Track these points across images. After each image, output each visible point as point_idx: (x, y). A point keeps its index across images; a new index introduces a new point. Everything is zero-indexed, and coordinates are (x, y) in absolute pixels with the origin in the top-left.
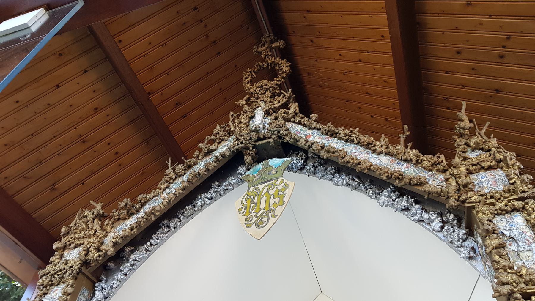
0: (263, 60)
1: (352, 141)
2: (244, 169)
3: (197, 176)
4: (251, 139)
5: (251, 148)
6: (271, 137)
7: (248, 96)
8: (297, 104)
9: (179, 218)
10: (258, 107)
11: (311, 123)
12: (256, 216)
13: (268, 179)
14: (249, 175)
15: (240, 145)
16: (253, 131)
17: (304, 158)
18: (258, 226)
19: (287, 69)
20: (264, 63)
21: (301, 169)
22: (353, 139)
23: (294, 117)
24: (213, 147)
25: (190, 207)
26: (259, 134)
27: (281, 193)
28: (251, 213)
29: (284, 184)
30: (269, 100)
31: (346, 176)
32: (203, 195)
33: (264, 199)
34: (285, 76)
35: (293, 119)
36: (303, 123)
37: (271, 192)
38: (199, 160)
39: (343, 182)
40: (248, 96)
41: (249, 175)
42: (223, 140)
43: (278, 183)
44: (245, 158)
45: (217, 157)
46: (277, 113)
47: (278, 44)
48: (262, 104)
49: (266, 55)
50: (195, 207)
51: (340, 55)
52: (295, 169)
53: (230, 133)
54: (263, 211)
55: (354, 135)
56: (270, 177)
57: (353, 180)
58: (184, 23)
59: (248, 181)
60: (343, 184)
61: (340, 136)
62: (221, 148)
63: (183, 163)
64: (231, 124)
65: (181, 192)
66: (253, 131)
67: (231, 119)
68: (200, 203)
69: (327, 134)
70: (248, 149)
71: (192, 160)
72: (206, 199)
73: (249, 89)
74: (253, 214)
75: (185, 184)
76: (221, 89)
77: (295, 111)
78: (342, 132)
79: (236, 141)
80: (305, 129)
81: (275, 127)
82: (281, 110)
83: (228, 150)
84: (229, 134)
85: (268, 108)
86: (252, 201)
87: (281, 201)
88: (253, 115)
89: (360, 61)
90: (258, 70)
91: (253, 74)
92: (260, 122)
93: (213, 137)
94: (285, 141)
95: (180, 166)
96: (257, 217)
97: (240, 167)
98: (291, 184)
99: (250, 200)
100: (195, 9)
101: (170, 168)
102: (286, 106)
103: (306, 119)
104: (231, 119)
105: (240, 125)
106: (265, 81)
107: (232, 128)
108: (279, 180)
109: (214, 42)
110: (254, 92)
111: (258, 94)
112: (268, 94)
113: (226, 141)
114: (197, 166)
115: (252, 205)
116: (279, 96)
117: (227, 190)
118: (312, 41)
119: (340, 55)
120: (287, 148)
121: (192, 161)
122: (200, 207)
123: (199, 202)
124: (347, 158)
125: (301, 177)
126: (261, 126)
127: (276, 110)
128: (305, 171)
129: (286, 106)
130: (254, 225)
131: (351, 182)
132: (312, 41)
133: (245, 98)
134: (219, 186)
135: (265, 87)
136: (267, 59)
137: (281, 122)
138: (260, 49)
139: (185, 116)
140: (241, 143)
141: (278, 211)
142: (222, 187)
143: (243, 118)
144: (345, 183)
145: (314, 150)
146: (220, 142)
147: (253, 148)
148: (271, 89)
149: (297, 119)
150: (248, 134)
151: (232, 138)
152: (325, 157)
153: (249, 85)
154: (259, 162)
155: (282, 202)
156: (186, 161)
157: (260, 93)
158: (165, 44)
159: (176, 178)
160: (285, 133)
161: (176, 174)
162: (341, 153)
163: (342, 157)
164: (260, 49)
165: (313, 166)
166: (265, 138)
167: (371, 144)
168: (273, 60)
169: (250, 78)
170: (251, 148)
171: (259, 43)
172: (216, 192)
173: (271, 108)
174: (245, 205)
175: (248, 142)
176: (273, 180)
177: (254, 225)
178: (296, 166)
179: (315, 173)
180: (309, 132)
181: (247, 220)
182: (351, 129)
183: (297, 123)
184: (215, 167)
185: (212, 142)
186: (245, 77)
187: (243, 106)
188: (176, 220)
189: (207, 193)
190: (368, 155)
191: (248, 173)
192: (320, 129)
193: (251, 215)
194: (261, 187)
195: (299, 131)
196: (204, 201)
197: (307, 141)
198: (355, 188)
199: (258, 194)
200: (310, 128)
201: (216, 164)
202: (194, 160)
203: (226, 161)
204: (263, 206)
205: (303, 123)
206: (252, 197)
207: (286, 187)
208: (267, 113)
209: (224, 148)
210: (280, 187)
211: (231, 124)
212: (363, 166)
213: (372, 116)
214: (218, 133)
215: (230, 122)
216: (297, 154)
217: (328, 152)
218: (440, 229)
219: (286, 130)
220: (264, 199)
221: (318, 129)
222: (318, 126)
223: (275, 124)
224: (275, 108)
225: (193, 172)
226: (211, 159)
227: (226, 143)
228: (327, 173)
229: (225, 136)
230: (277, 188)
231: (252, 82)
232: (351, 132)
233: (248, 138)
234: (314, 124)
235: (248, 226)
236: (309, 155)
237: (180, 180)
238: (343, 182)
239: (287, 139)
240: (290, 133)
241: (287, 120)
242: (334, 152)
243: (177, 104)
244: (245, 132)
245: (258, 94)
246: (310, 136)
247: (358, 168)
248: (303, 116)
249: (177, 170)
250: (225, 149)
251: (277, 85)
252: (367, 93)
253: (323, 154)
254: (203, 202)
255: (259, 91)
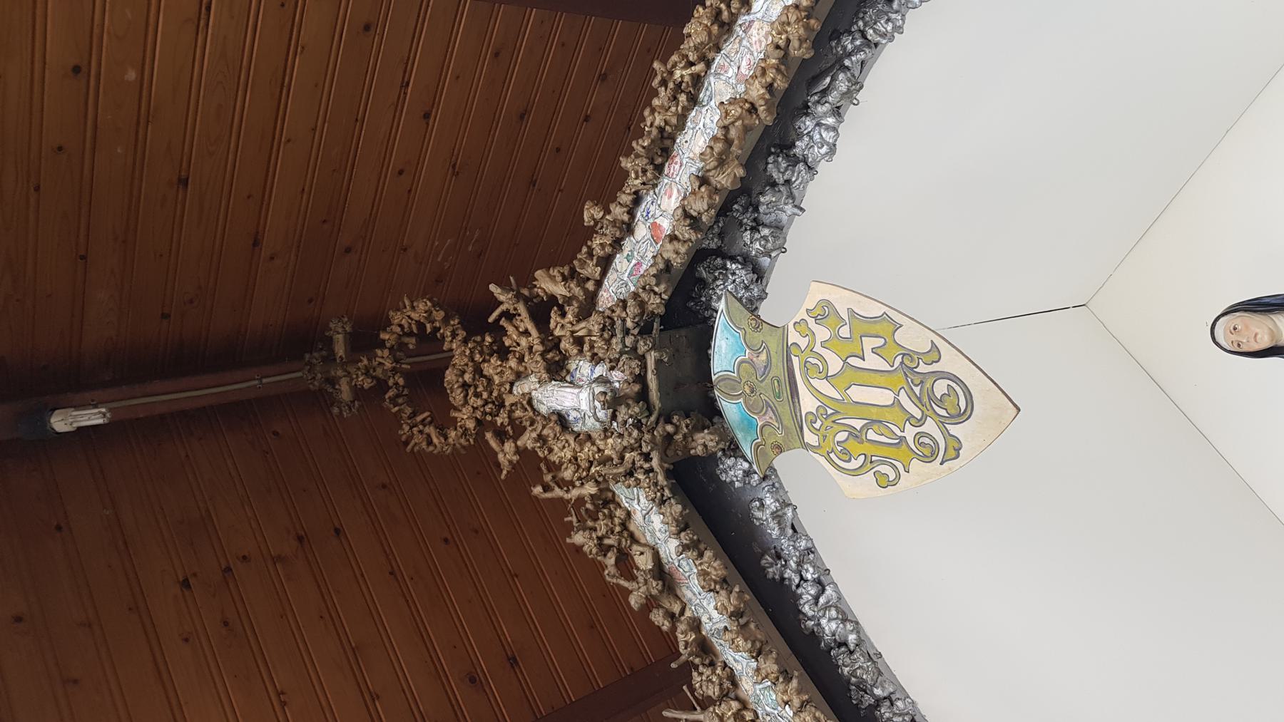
0: (382, 386)
1: (698, 80)
2: (730, 462)
3: (742, 621)
4: (638, 425)
5: (670, 428)
6: (642, 358)
7: (489, 436)
8: (538, 274)
9: (879, 702)
10: (530, 402)
11: (614, 223)
12: (921, 422)
13: (784, 377)
14: (758, 446)
15: (655, 463)
16: (614, 417)
17: (719, 261)
18: (960, 415)
19: (421, 306)
20: (391, 382)
21: (759, 274)
22: (691, 75)
23: (583, 281)
24: (644, 562)
25: (843, 659)
26: (626, 397)
27: (845, 332)
28: (902, 439)
29: (811, 321)
30: (513, 363)
31: (807, 114)
32: (806, 609)
33: (857, 394)
34: (442, 313)
35: (590, 286)
36: (608, 250)
37: (835, 365)
38: (682, 612)
39: (828, 128)
40: (489, 436)
41: (758, 446)
42: (624, 525)
43: (803, 343)
44: (699, 451)
45: (685, 548)
46: (559, 339)
47: (339, 339)
48: (527, 386)
49: (367, 374)
50: (845, 644)
51: (401, 172)
52: (756, 292)
53: (606, 501)
54: (903, 398)
55: (678, 73)
56: (778, 370)
57: (825, 92)
58: (226, 624)
59: (779, 449)
60: (835, 129)
61: (674, 121)
62: (653, 533)
63: (688, 667)
64: (575, 493)
65: (794, 683)
66: (614, 417)
67: (558, 492)
68: (833, 625)
69: (659, 169)
70: (669, 438)
71: (680, 637)
72: (822, 600)
73: (465, 431)
74: (910, 433)
75: (770, 666)
76: (446, 540)
77: (565, 279)
78: (654, 120)
79: (638, 482)
80: (628, 244)
81: (608, 342)
82: (552, 325)
83: (665, 509)
84: (606, 503)
85: (541, 364)
86: (855, 435)
87: (877, 328)
88: (554, 418)
89: (427, 116)
90: (410, 402)
91: (419, 418)
92: (585, 395)
93: (610, 560)
94: (661, 310)
95: (696, 678)
96: (932, 407)
97: (723, 477)
98: (817, 293)
99: (852, 445)
100: (186, 584)
101: (701, 717)
102: (542, 310)
103: (597, 242)
104: (558, 492)
105: (584, 464)
106: (450, 375)
107: (590, 489)
108: (793, 337)
109: (300, 539)
110: (478, 414)
111: (486, 403)
112: (491, 368)
113: (629, 514)
114: (704, 619)
115: (871, 435)
116: (504, 331)
117: (793, 527)
118: (348, 250)
119: (401, 172)
120: (681, 313)
121: (684, 637)
122: (849, 627)
123: (829, 626)
124: (757, 91)
125: (781, 273)
126: (598, 389)
127: (552, 344)
128: (765, 261)
129: (542, 310)
130: (953, 430)
131: (833, 97)
132: (348, 250)
133: (493, 444)
134: (778, 556)
135: (467, 377)
136: (379, 372)
137: (594, 323)
138: (345, 392)
139: (513, 661)
140: (647, 457)
141: (913, 338)
142: (785, 543)
143: (562, 452)
144: (830, 121)
145: (710, 207)
146: (632, 535)
147: (668, 421)
148: (478, 357)
149: (591, 270)
150: (621, 436)
151: (622, 492)
152: (740, 172)
153: (453, 434)
154: (719, 413)
155: (886, 326)
156: (683, 658)
157: (485, 395)
158: (279, 694)
159: (737, 699)
160: (632, 309)
161: (724, 696)
162: (735, 111)
163: (749, 111)
164: (345, 392)
165: (754, 229)
166: (641, 379)
167: (719, 12)
168: (386, 352)
169: (431, 430)
170: (670, 428)
171: (321, 399)
172: (799, 564)
173: (543, 355)
174: (869, 461)
175: (647, 437)
176: (789, 360)
177: (953, 430)
178: (746, 288)
179: (778, 228)
180: (641, 231)
181: (929, 457)
182: (655, 83)
183: (604, 273)
184: (716, 557)
185: (625, 564)
186: (424, 445)
187: (518, 451)
188: (885, 711)
189: (800, 597)
190: (756, 25)
191: (747, 449)
192: (636, 193)
193: (910, 440)
194: (808, 403)
195: (629, 272)
196: (827, 607)
197: (673, 238)
198: (856, 85)
199: (831, 413)
200: (629, 229)
201: (708, 554)
202: (682, 627)
203: (698, 520)
204: (883, 397)
205: (608, 250)
206: (842, 436)
207: (824, 313)
208: (557, 370)
209: (653, 521)
210: (822, 333)
211: (575, 493)
212: (795, 31)
213: (587, 119)
214: (600, 539)
215: (567, 496)
216: (703, 284)
217: (721, 162)
218: (801, 166)
219: (625, 308)
220: (857, 394)
221: (637, 200)
222: (625, 198)
223: (600, 343)
224: (542, 343)
225: (728, 636)
226: (688, 571)
227: (638, 517)
228: (788, 182)
229: (611, 516)
230: (823, 345)
231: (444, 422)
232: (664, 83)
233: (635, 433)
234: (618, 212)
235: (955, 449)
236: (713, 246)
237: (747, 686)
238: (828, 128)
239: (654, 303)
240: (635, 295)
241: (588, 307)
242: (728, 142)
243: (473, 680)
244: (610, 446)
245: (486, 403)
246: (655, 227)
247: (799, 51)
248: (585, 249)
249: (713, 691)
250: (657, 520)
251: (465, 341)
252: (522, 117)
253: (724, 180)
254: (833, 613)
255: (477, 395)
